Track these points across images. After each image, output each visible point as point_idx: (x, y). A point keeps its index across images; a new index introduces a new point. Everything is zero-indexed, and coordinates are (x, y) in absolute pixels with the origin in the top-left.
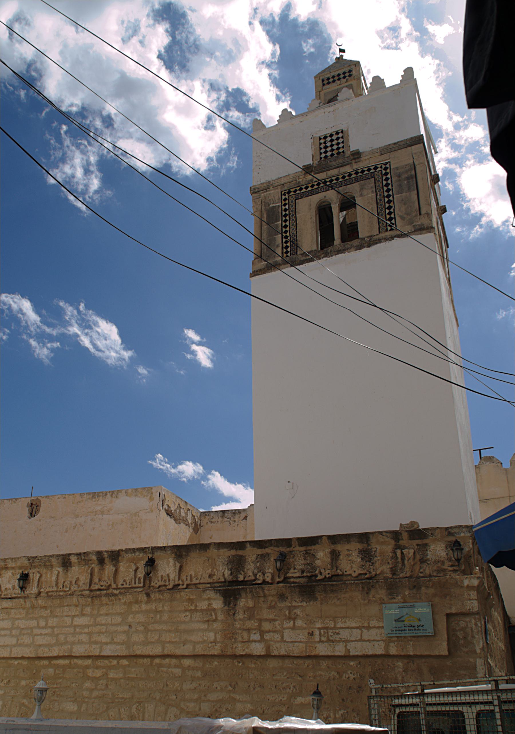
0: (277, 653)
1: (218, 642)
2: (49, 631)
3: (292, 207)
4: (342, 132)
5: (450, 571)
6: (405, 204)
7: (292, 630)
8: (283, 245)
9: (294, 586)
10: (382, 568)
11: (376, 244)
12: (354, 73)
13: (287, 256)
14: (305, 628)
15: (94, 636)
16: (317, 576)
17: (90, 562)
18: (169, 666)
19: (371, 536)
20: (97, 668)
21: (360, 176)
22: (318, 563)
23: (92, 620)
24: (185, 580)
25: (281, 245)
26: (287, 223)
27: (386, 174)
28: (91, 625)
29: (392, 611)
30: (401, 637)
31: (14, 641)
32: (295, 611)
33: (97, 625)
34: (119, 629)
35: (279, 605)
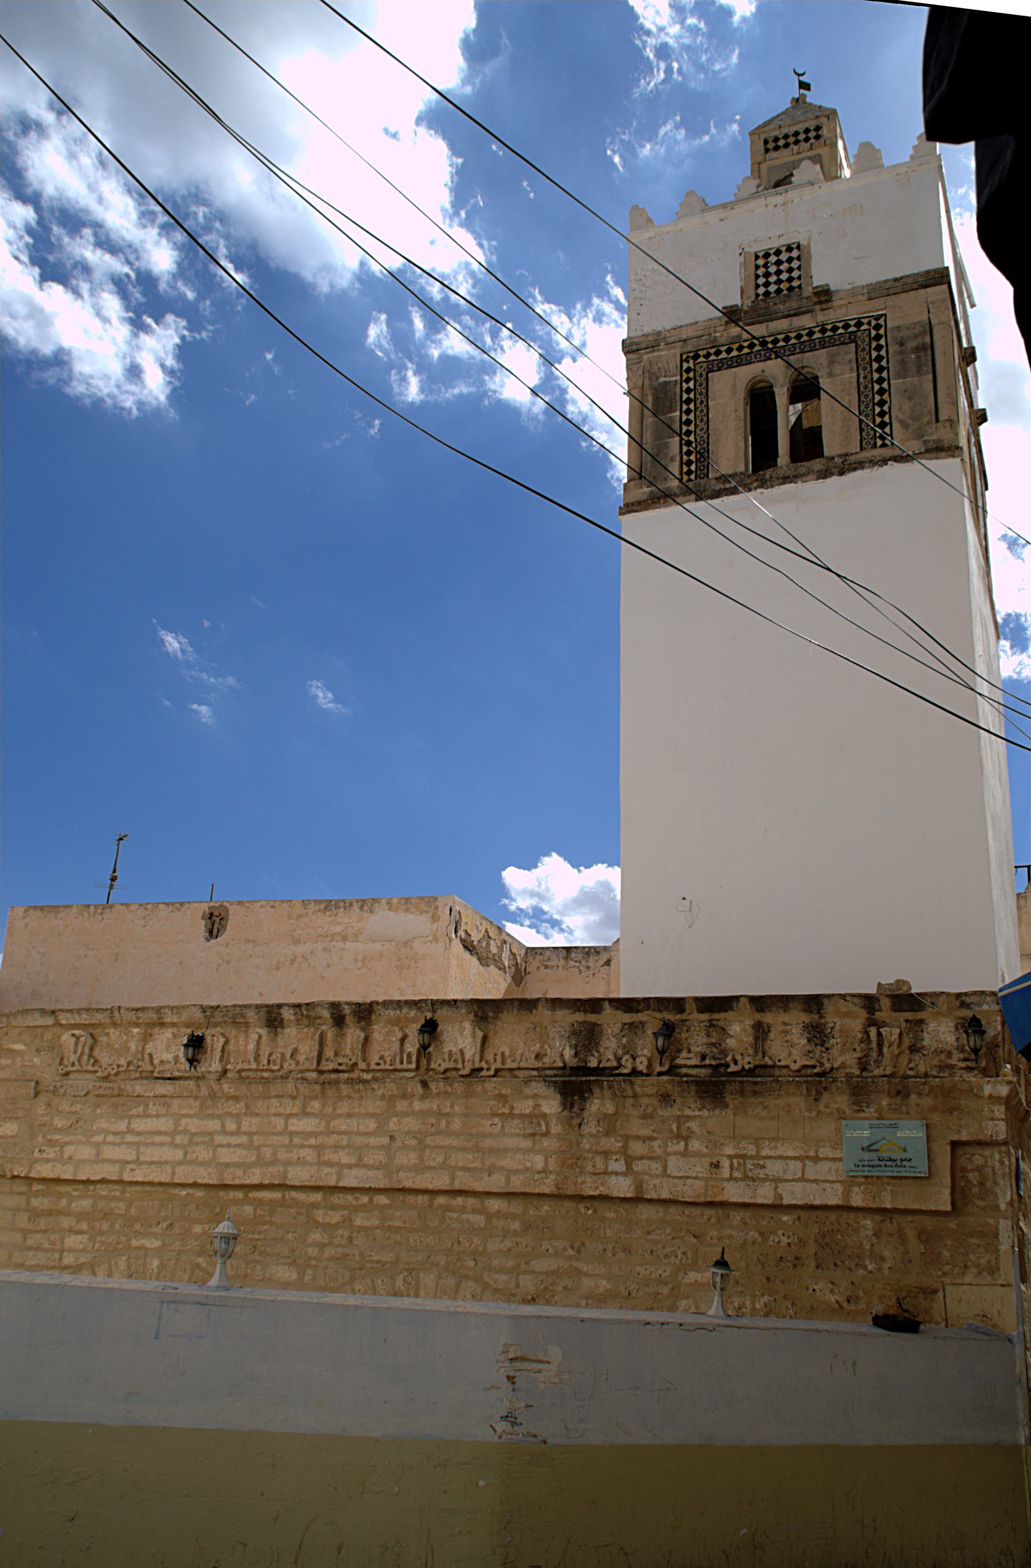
0: (654, 1196)
1: (551, 1172)
2: (243, 1139)
3: (700, 385)
4: (798, 247)
5: (962, 1068)
6: (910, 398)
7: (685, 1155)
8: (681, 458)
9: (687, 1082)
10: (843, 1057)
11: (855, 469)
12: (824, 132)
13: (690, 480)
14: (705, 1155)
15: (327, 1152)
16: (727, 1066)
17: (318, 1021)
18: (463, 1210)
19: (825, 1001)
20: (333, 1207)
21: (830, 337)
22: (731, 1043)
23: (323, 1123)
24: (492, 1060)
25: (678, 459)
26: (692, 417)
27: (878, 337)
28: (321, 1133)
29: (861, 1131)
30: (872, 1177)
31: (179, 1155)
32: (687, 1125)
33: (332, 1133)
34: (372, 1141)
35: (660, 1112)
